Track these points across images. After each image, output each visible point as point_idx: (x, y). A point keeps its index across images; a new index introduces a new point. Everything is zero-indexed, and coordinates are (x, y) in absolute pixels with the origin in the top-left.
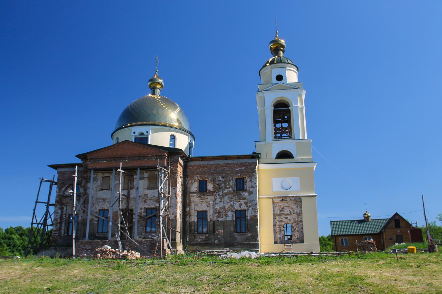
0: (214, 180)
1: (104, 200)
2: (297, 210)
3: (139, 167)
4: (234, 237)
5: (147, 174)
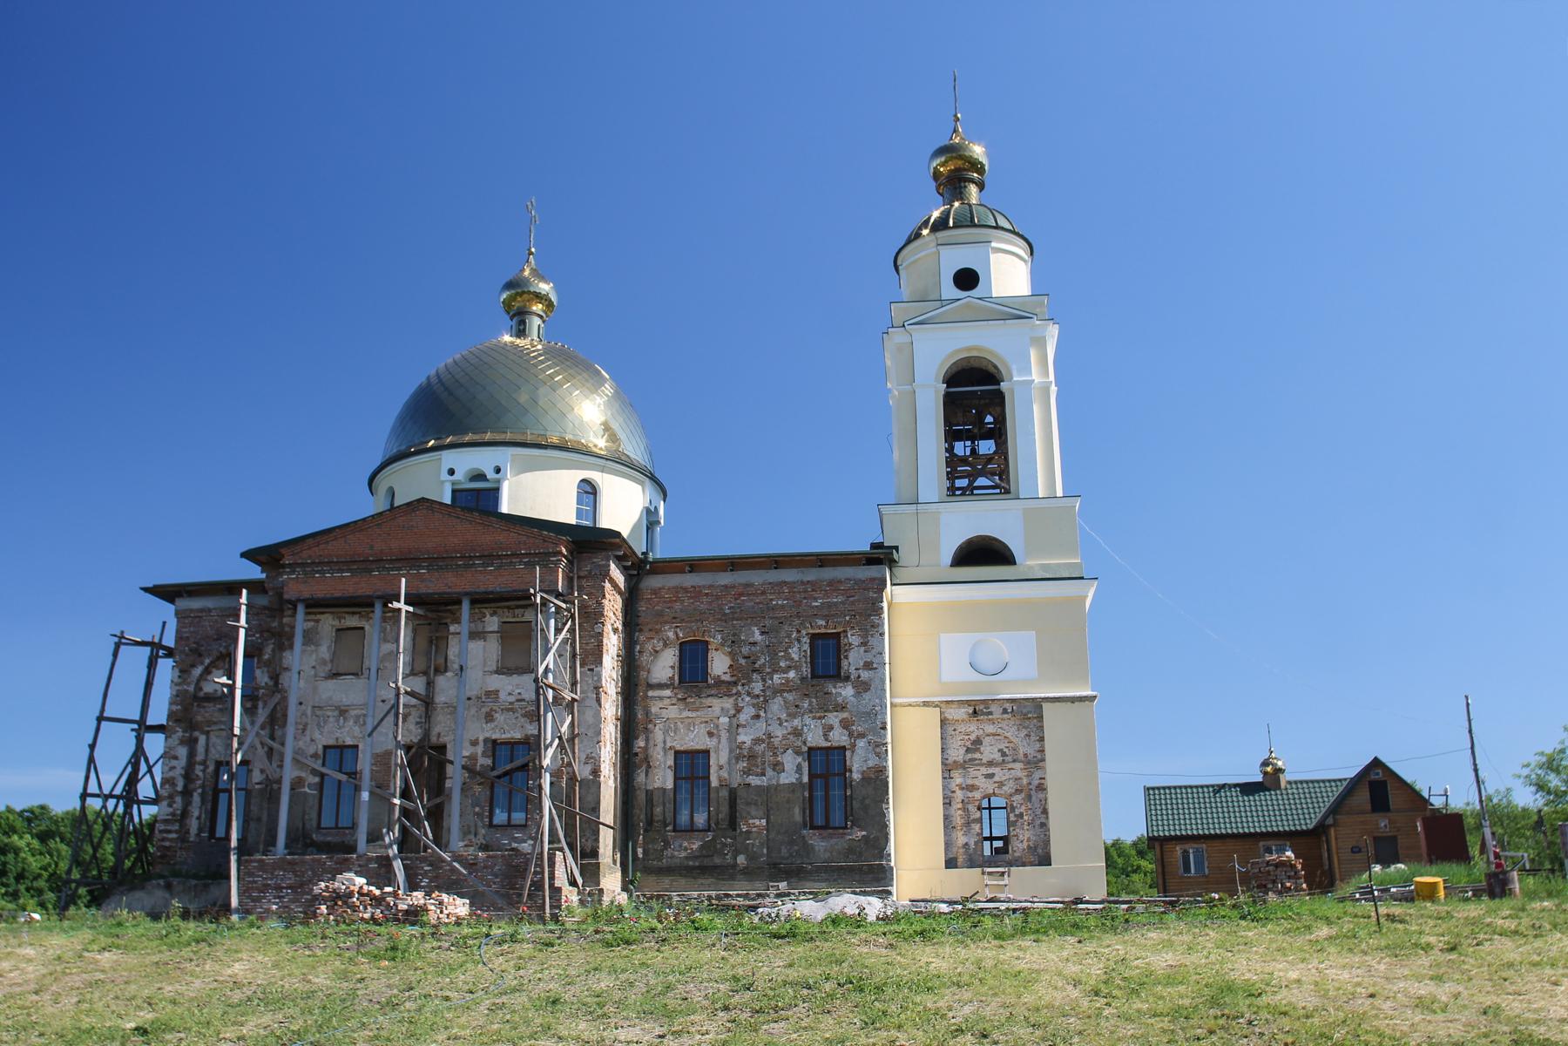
0: (733, 643)
1: (343, 712)
2: (1026, 748)
3: (467, 594)
4: (805, 843)
5: (495, 619)
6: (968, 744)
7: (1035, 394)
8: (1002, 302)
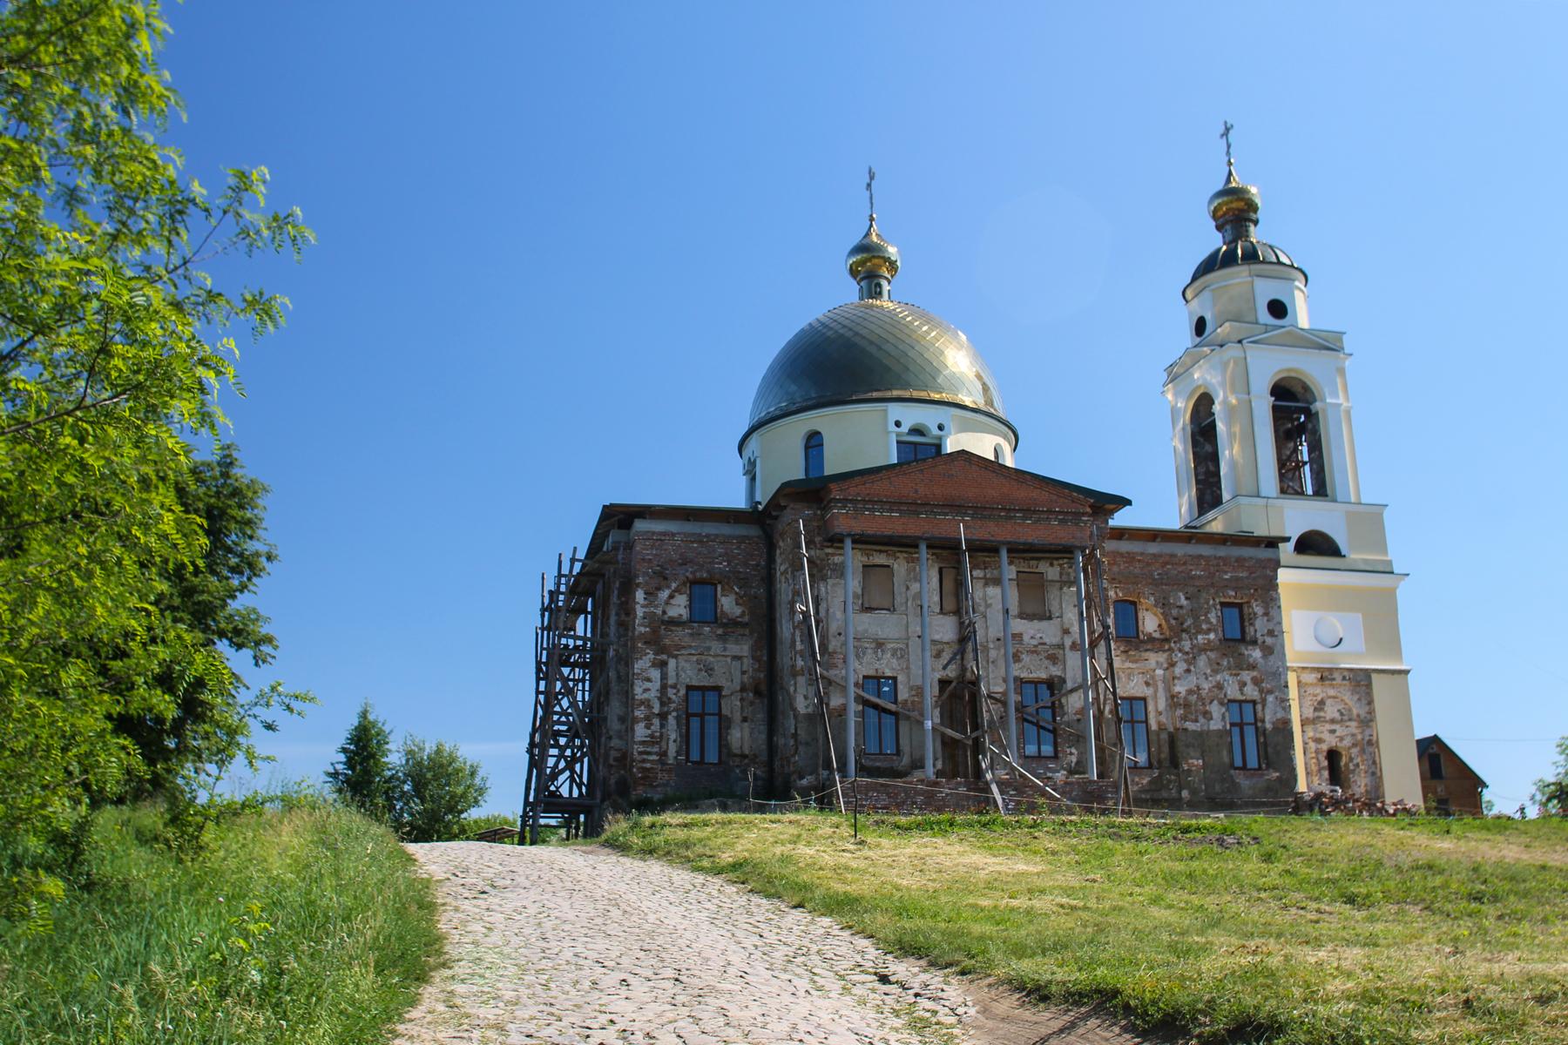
0: (1164, 604)
1: (879, 645)
2: (1358, 710)
3: (849, 535)
4: (1233, 781)
5: (1013, 568)
7: (1343, 415)
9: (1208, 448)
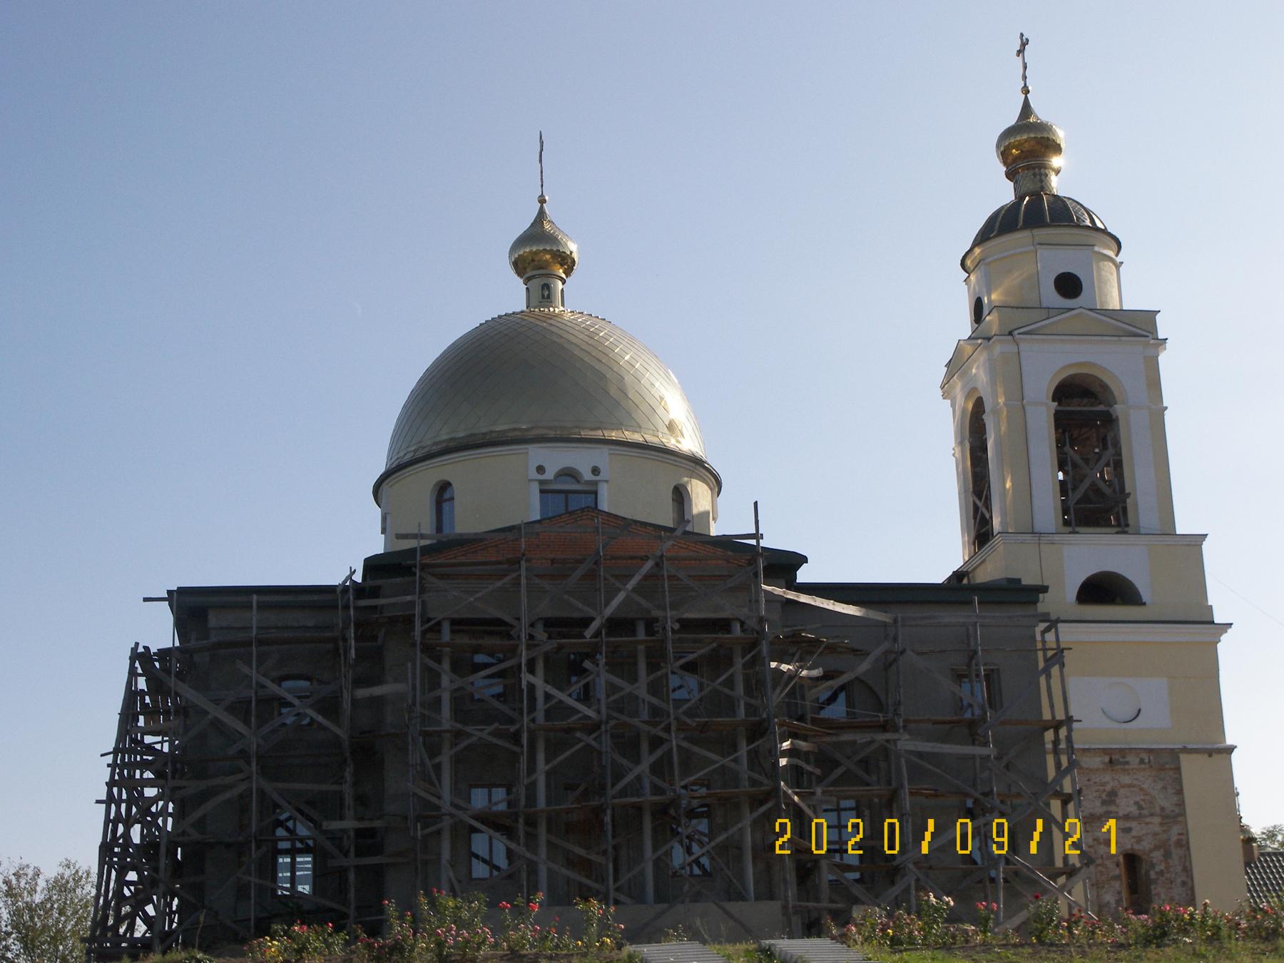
6: (1104, 796)
8: (1120, 315)
9: (978, 469)
